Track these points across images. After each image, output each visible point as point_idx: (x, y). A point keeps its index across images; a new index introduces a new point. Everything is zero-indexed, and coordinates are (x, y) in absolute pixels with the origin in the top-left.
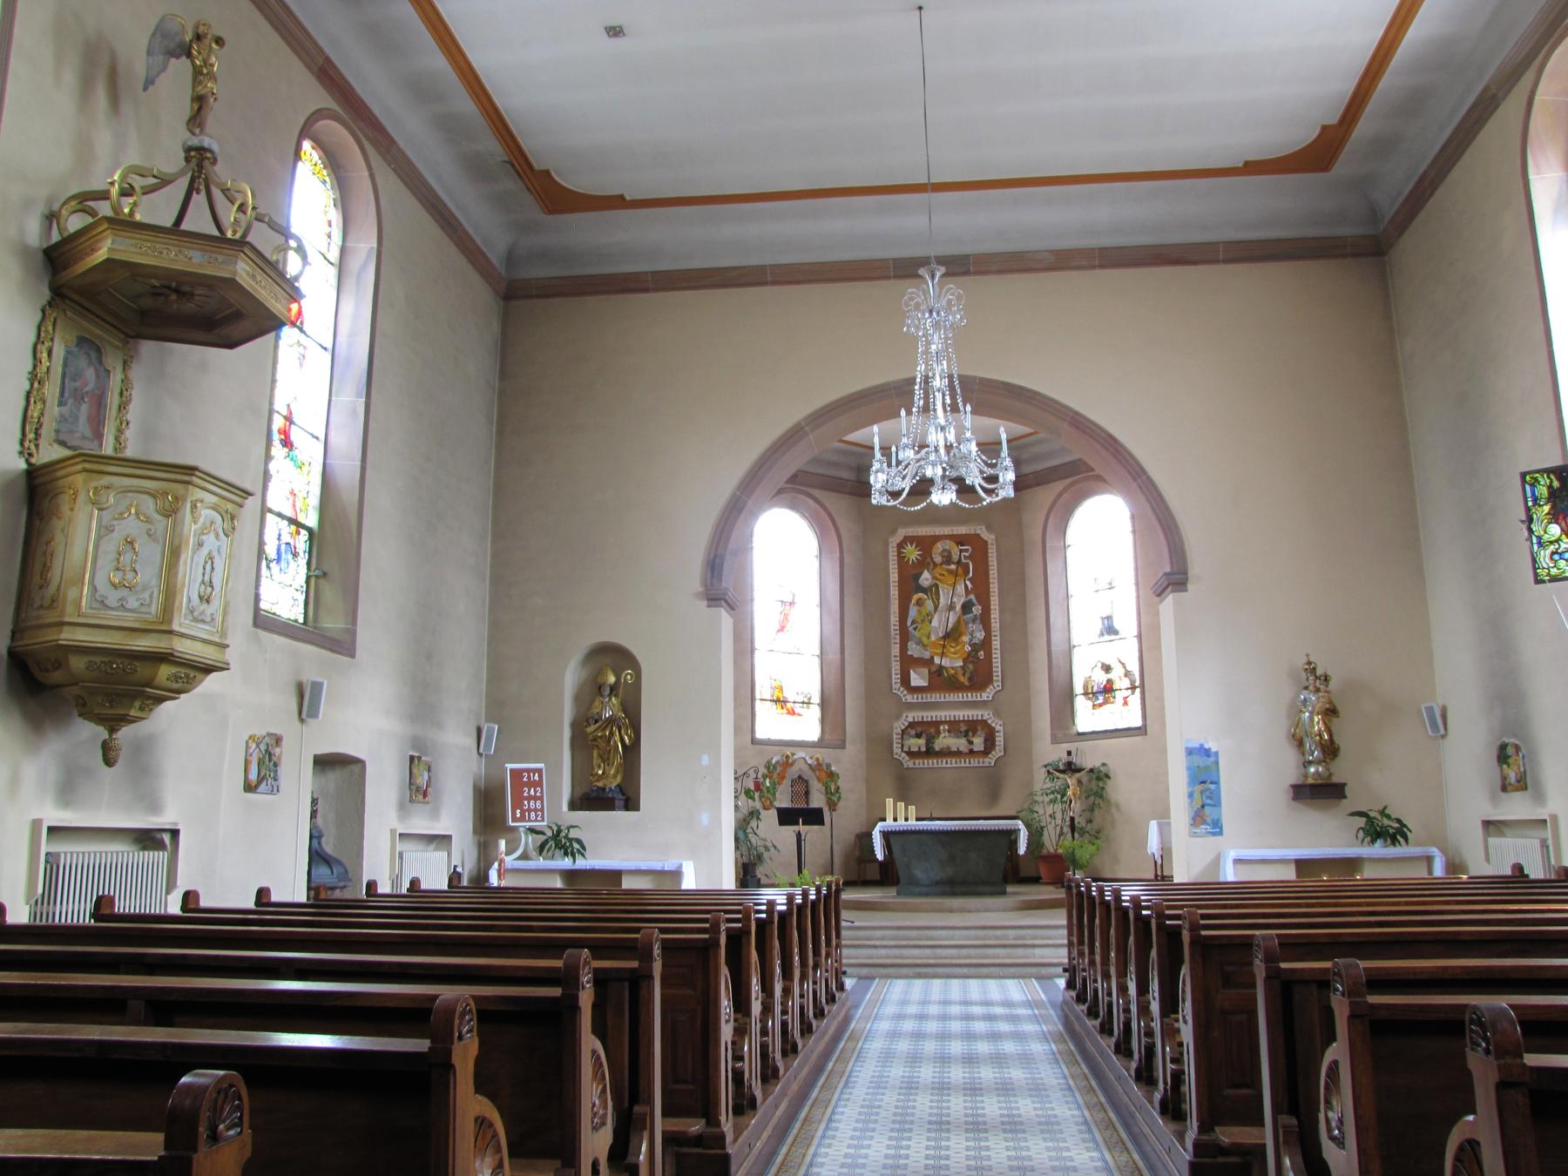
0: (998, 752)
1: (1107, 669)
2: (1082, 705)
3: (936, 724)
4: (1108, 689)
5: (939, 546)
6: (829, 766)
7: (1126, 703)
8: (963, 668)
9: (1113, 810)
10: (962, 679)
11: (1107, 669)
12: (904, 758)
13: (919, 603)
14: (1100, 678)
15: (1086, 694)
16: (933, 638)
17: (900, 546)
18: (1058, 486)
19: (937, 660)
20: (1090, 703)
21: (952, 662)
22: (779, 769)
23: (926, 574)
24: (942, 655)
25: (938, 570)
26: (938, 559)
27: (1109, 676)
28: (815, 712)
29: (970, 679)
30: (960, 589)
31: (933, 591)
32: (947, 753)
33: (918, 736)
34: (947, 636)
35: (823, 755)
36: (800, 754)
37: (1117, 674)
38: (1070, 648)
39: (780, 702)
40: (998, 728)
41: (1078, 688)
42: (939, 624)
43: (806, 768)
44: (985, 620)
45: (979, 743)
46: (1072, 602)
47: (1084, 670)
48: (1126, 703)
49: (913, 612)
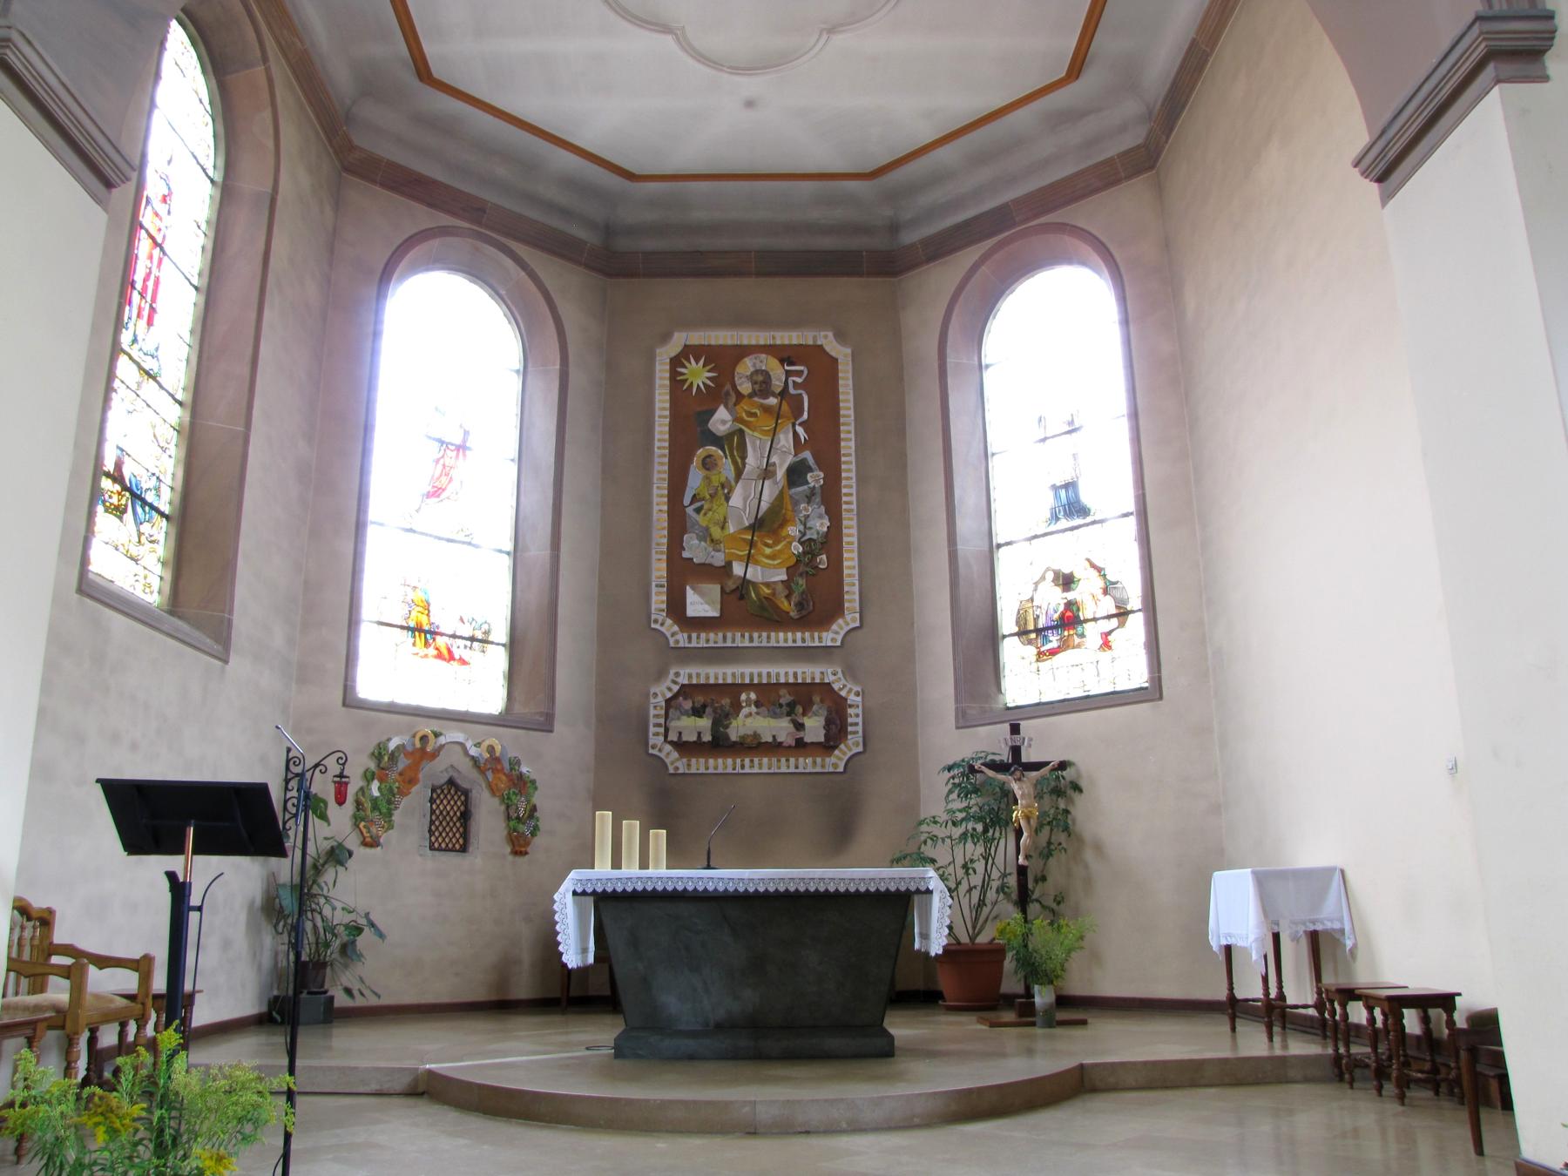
0: (852, 744)
1: (1067, 582)
2: (1015, 655)
3: (733, 690)
4: (1070, 620)
5: (747, 366)
6: (515, 763)
7: (1106, 645)
8: (786, 584)
9: (1089, 855)
10: (785, 605)
11: (1067, 582)
12: (670, 756)
13: (708, 463)
14: (1052, 600)
15: (1022, 633)
16: (731, 529)
17: (676, 362)
18: (967, 257)
19: (738, 569)
20: (1031, 651)
21: (766, 573)
22: (403, 763)
23: (722, 413)
24: (749, 559)
25: (745, 405)
26: (745, 387)
27: (1070, 596)
28: (498, 660)
29: (800, 605)
30: (785, 440)
31: (734, 443)
32: (753, 746)
33: (698, 712)
34: (758, 525)
35: (504, 742)
36: (453, 735)
37: (1088, 595)
38: (992, 549)
39: (423, 632)
40: (852, 698)
41: (1007, 624)
42: (743, 502)
43: (465, 766)
44: (830, 498)
45: (814, 726)
46: (994, 464)
47: (1019, 586)
48: (1106, 645)
49: (695, 478)
